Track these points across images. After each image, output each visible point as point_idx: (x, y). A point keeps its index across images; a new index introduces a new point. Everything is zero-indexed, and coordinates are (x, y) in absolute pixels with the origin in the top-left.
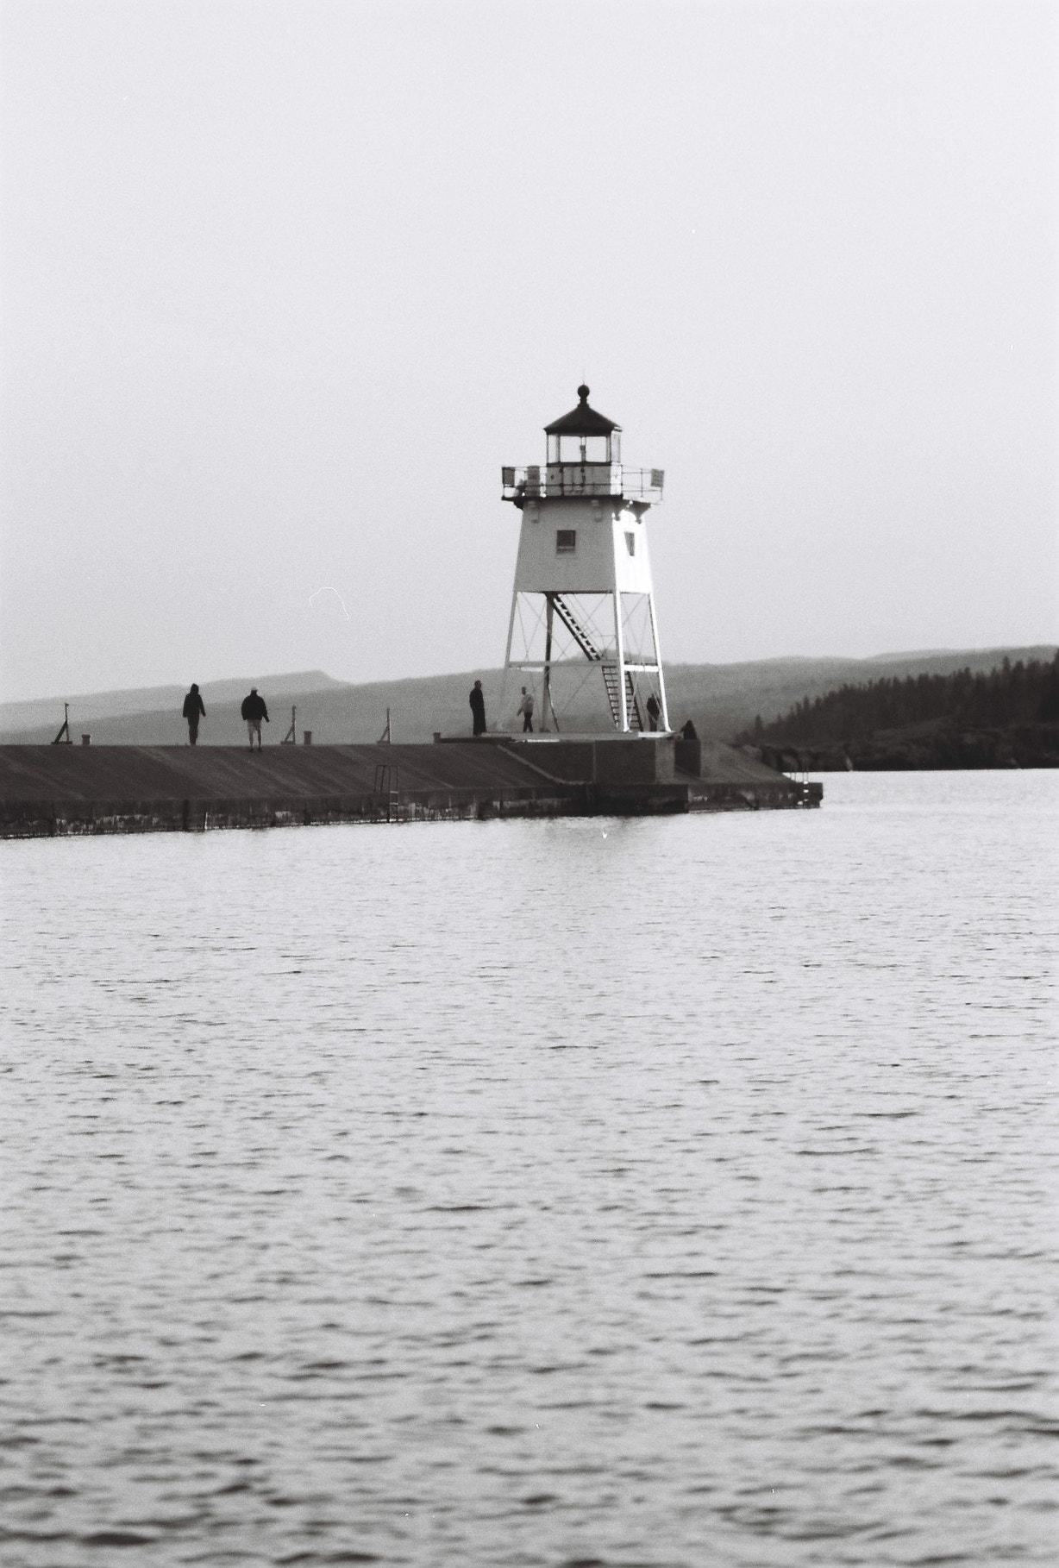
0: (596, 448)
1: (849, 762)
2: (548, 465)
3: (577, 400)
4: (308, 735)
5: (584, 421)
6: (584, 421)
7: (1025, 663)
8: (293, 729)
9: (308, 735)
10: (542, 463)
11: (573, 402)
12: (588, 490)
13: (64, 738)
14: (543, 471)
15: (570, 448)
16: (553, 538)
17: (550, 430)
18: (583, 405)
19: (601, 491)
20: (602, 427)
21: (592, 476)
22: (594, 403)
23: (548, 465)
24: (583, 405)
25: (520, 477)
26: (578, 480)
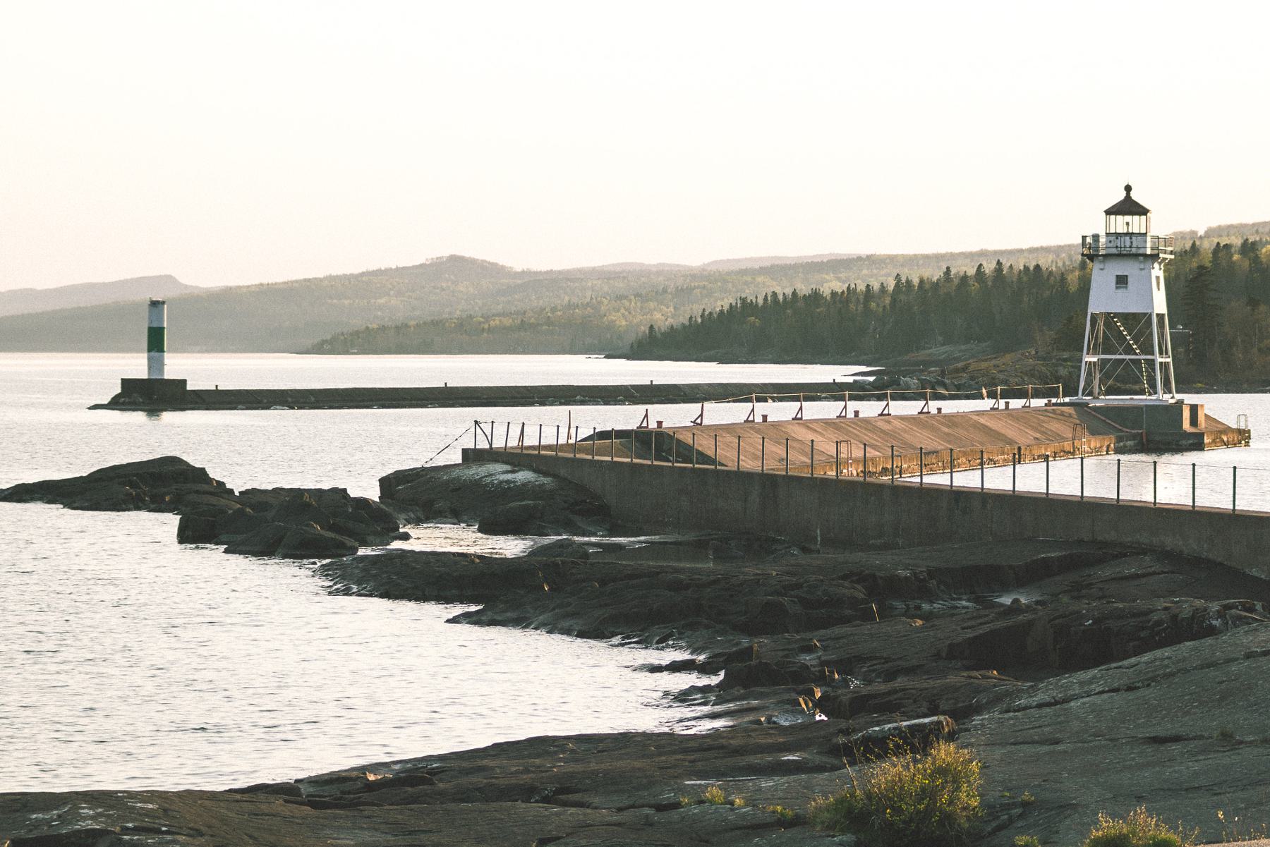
0: (1136, 223)
1: (370, 538)
2: (1108, 234)
3: (1124, 194)
4: (660, 423)
5: (1128, 207)
6: (1128, 207)
7: (989, 267)
8: (701, 415)
9: (660, 423)
10: (1102, 233)
11: (1122, 195)
12: (1134, 250)
13: (644, 424)
14: (1103, 240)
15: (1120, 223)
16: (1114, 280)
17: (1108, 212)
18: (1128, 197)
19: (1141, 251)
20: (1143, 211)
21: (1136, 242)
22: (1134, 195)
23: (1108, 234)
24: (1128, 197)
25: (1089, 240)
26: (1128, 244)
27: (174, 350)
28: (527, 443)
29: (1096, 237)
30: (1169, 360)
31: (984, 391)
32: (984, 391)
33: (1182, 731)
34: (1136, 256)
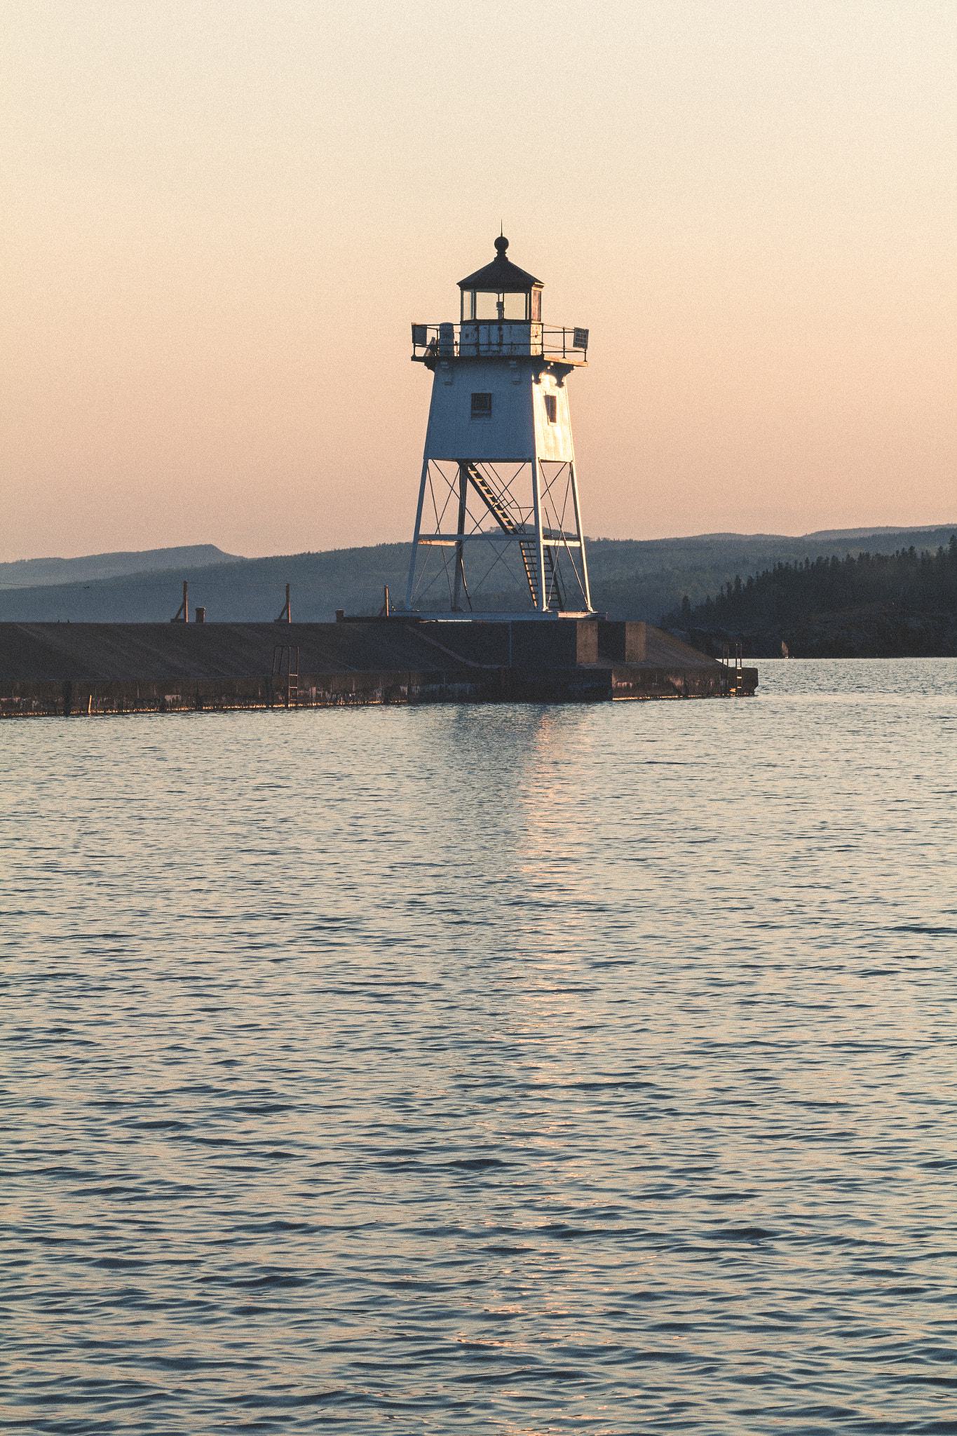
0: (515, 306)
3: (494, 253)
5: (502, 275)
6: (502, 275)
14: (457, 329)
15: (487, 304)
16: (467, 403)
17: (464, 285)
19: (520, 351)
22: (512, 255)
23: (463, 323)
25: (432, 334)
26: (495, 339)
27: (941, 531)
28: (427, 528)
29: (446, 329)
30: (544, 542)
31: (784, 647)
32: (784, 647)
33: (275, 941)
34: (504, 360)
